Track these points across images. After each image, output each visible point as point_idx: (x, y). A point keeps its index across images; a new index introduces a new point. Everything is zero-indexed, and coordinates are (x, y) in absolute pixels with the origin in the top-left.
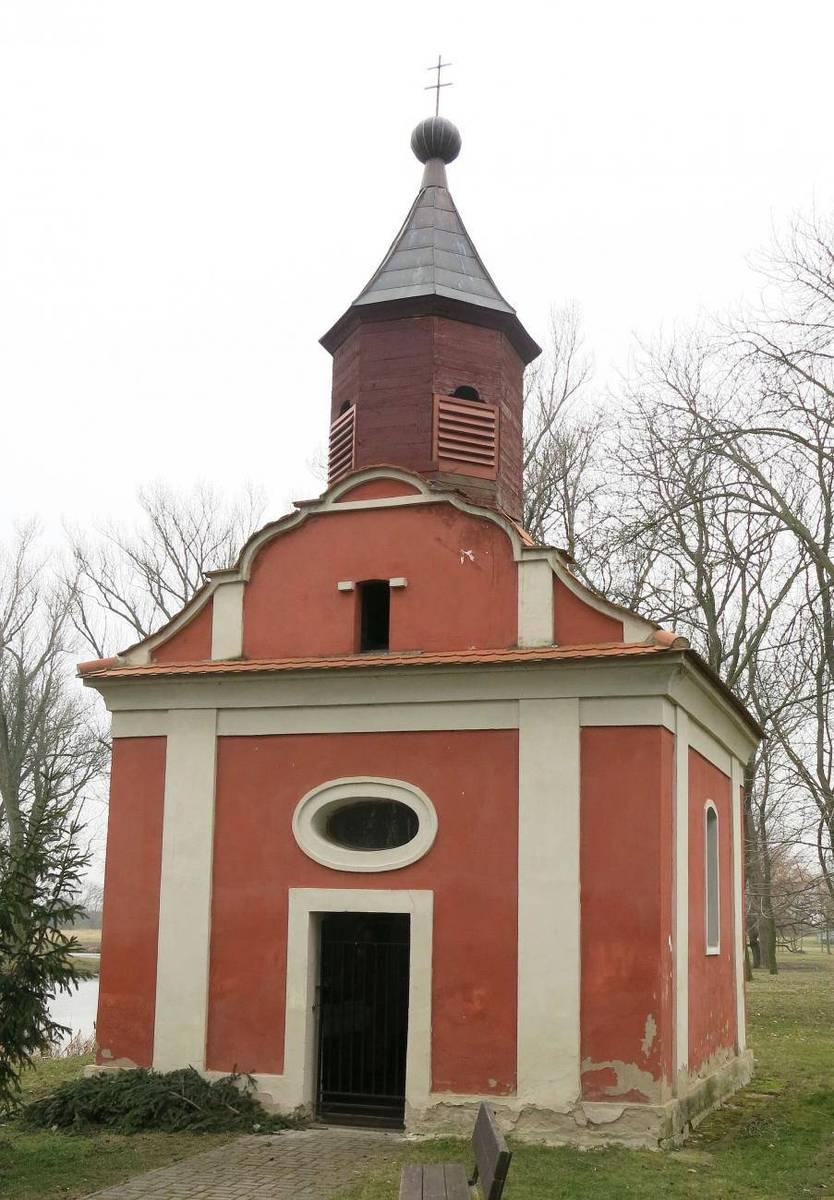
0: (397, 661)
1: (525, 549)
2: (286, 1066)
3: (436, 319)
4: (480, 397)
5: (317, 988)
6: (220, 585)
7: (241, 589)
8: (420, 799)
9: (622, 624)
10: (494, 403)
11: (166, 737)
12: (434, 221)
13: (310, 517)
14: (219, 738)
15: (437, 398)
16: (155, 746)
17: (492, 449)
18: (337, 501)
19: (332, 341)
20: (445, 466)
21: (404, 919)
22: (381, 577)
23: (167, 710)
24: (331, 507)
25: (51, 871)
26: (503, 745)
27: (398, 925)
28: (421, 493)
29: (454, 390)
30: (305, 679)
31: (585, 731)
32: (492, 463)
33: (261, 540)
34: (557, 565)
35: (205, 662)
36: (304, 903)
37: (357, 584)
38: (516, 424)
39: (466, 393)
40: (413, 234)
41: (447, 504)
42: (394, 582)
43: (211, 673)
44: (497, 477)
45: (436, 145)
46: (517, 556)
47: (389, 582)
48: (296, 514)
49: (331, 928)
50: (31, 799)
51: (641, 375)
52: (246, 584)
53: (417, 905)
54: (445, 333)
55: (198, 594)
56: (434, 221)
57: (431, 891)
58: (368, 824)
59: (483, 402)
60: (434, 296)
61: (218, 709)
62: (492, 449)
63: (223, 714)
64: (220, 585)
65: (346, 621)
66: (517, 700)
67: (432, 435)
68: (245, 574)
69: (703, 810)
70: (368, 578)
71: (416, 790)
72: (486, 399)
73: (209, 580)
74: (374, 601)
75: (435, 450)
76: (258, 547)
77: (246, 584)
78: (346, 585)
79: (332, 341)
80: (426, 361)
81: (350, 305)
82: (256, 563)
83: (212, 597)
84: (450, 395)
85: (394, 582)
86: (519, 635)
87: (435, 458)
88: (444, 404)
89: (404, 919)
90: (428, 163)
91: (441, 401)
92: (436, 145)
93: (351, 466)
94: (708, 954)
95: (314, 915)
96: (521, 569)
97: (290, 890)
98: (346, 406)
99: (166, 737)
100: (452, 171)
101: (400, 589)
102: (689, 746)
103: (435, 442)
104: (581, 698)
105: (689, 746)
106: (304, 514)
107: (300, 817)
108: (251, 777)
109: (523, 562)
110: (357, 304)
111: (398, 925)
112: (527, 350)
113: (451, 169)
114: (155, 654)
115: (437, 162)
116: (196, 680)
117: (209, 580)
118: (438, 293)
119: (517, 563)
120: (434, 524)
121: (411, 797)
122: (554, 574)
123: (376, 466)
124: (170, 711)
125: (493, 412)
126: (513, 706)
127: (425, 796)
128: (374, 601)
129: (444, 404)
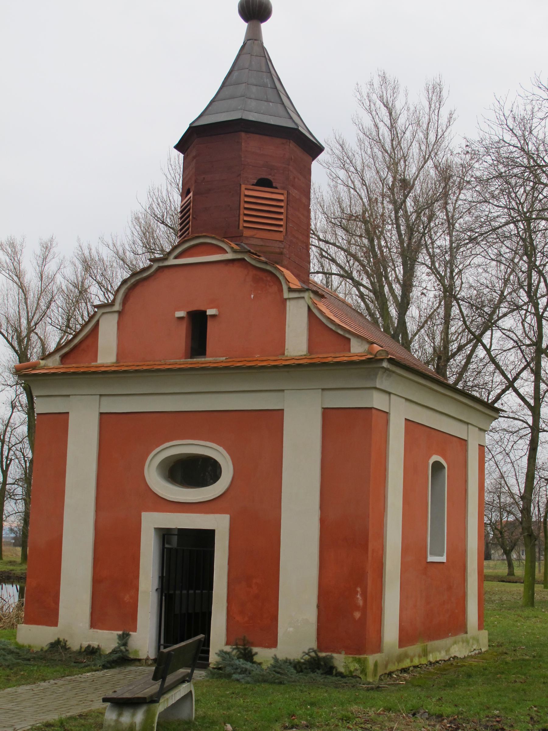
0: (330, 359)
1: (290, 290)
3: (243, 134)
4: (274, 185)
5: (159, 577)
6: (103, 313)
7: (116, 316)
8: (224, 457)
9: (349, 340)
10: (283, 188)
13: (160, 268)
14: (101, 414)
15: (243, 187)
16: (61, 420)
17: (281, 220)
18: (176, 258)
19: (181, 146)
20: (247, 233)
21: (211, 533)
22: (203, 309)
23: (69, 396)
24: (172, 262)
27: (207, 537)
28: (227, 253)
29: (255, 181)
31: (326, 411)
32: (281, 229)
33: (129, 284)
34: (310, 300)
35: (93, 364)
36: (152, 522)
37: (189, 313)
38: (304, 200)
39: (264, 183)
40: (235, 74)
41: (243, 260)
42: (210, 312)
43: (168, 369)
44: (284, 238)
46: (286, 295)
47: (205, 312)
48: (150, 267)
49: (165, 535)
51: (540, 109)
52: (120, 313)
53: (219, 524)
54: (251, 145)
55: (91, 318)
58: (192, 471)
59: (276, 188)
60: (241, 120)
61: (101, 395)
62: (281, 220)
63: (103, 398)
64: (103, 313)
65: (180, 337)
67: (239, 212)
68: (117, 307)
69: (428, 463)
70: (195, 308)
71: (221, 449)
72: (278, 185)
73: (96, 310)
74: (198, 322)
75: (241, 222)
76: (127, 288)
77: (120, 313)
78: (181, 314)
79: (181, 146)
80: (244, 156)
81: (188, 126)
82: (125, 301)
83: (98, 321)
84: (253, 185)
85: (210, 312)
86: (286, 348)
87: (241, 228)
88: (249, 192)
89: (211, 533)
90: (249, 23)
91: (246, 189)
93: (188, 234)
94: (428, 561)
95: (158, 530)
96: (288, 303)
97: (143, 514)
98: (188, 192)
99: (68, 413)
101: (213, 316)
102: (406, 419)
103: (241, 217)
104: (323, 390)
105: (406, 419)
106: (156, 266)
107: (149, 466)
109: (289, 299)
110: (194, 125)
111: (207, 537)
112: (314, 149)
113: (265, 27)
114: (64, 357)
115: (255, 22)
116: (193, 373)
117: (96, 310)
118: (243, 118)
119: (286, 299)
120: (238, 271)
121: (208, 449)
122: (309, 308)
123: (200, 235)
125: (283, 194)
126: (280, 394)
127: (225, 451)
128: (198, 322)
129: (249, 192)
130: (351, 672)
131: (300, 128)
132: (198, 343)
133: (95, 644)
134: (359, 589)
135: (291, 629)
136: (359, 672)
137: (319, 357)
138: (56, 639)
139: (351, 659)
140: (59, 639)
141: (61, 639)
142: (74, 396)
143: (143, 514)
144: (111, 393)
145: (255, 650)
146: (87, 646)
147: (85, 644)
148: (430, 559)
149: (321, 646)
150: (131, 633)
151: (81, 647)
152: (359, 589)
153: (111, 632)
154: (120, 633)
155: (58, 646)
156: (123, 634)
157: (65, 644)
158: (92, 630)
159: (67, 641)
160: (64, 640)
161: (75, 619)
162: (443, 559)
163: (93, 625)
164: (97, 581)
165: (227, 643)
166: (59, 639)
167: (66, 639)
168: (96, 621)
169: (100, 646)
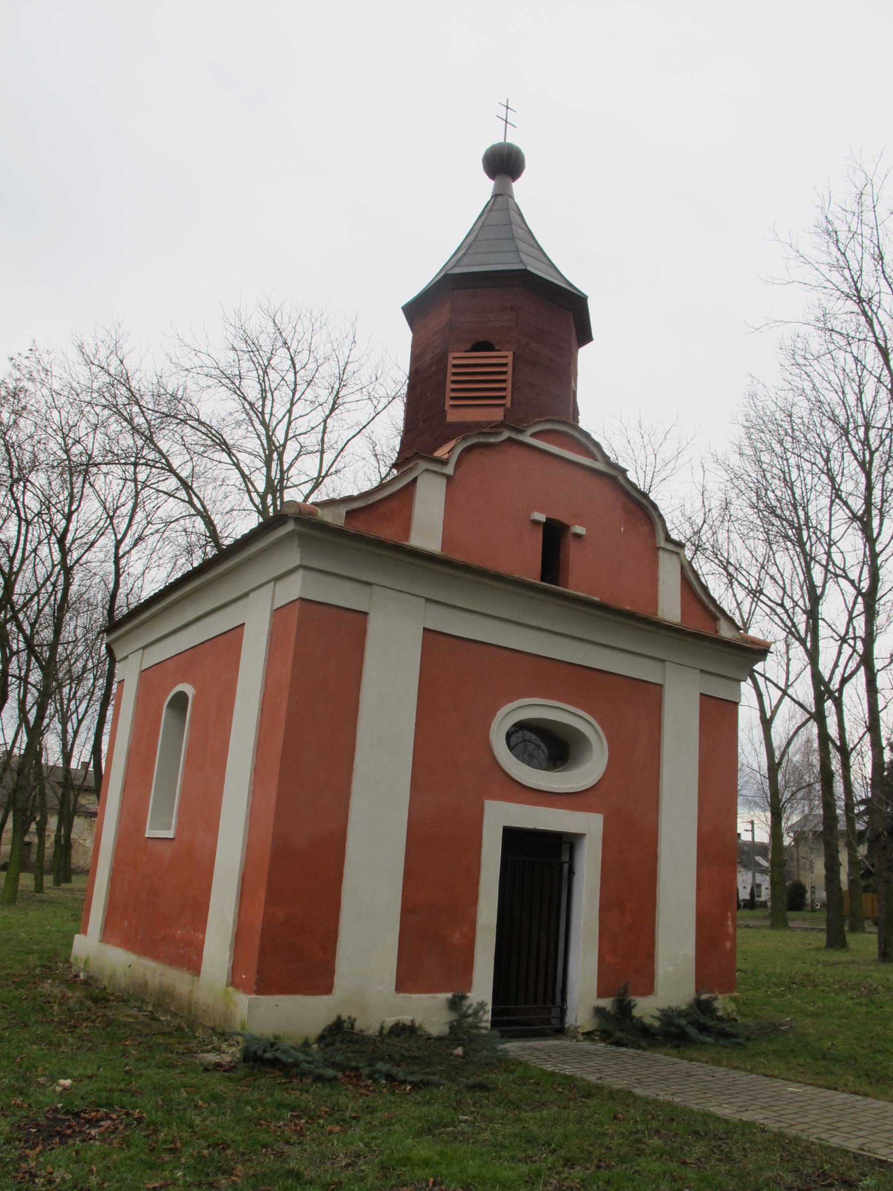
2: (337, 980)
6: (427, 470)
11: (366, 614)
12: (501, 220)
25: (862, 808)
26: (650, 696)
30: (250, 559)
36: (500, 816)
45: (504, 164)
49: (513, 838)
50: (29, 629)
53: (588, 825)
56: (501, 220)
57: (602, 816)
58: (554, 746)
66: (663, 661)
77: (448, 478)
85: (579, 530)
92: (504, 164)
100: (519, 188)
101: (578, 536)
108: (452, 677)
109: (664, 549)
124: (374, 586)
127: (504, 708)
130: (728, 1014)
131: (529, 268)
132: (553, 562)
133: (407, 1019)
134: (729, 914)
135: (671, 969)
136: (735, 1013)
137: (351, 529)
138: (334, 1018)
139: (728, 999)
140: (339, 1018)
141: (345, 1017)
142: (381, 588)
143: (602, 816)
144: (564, 632)
145: (633, 998)
146: (392, 1024)
147: (390, 1021)
148: (149, 833)
149: (699, 989)
150: (468, 994)
151: (382, 1028)
152: (729, 914)
153: (431, 995)
154: (449, 995)
155: (339, 1031)
156: (454, 996)
157: (353, 1025)
158: (401, 995)
159: (355, 1020)
160: (349, 1018)
161: (367, 977)
162: (170, 834)
163: (399, 988)
164: (408, 909)
165: (600, 995)
166: (339, 1018)
167: (353, 1017)
168: (407, 980)
169: (661, 1007)
